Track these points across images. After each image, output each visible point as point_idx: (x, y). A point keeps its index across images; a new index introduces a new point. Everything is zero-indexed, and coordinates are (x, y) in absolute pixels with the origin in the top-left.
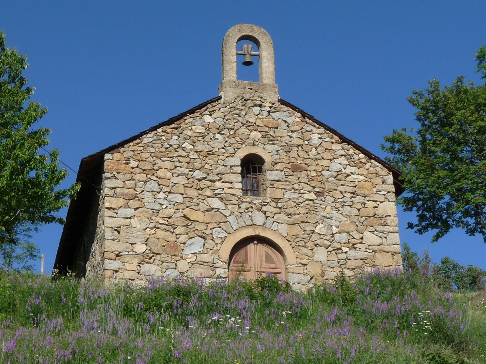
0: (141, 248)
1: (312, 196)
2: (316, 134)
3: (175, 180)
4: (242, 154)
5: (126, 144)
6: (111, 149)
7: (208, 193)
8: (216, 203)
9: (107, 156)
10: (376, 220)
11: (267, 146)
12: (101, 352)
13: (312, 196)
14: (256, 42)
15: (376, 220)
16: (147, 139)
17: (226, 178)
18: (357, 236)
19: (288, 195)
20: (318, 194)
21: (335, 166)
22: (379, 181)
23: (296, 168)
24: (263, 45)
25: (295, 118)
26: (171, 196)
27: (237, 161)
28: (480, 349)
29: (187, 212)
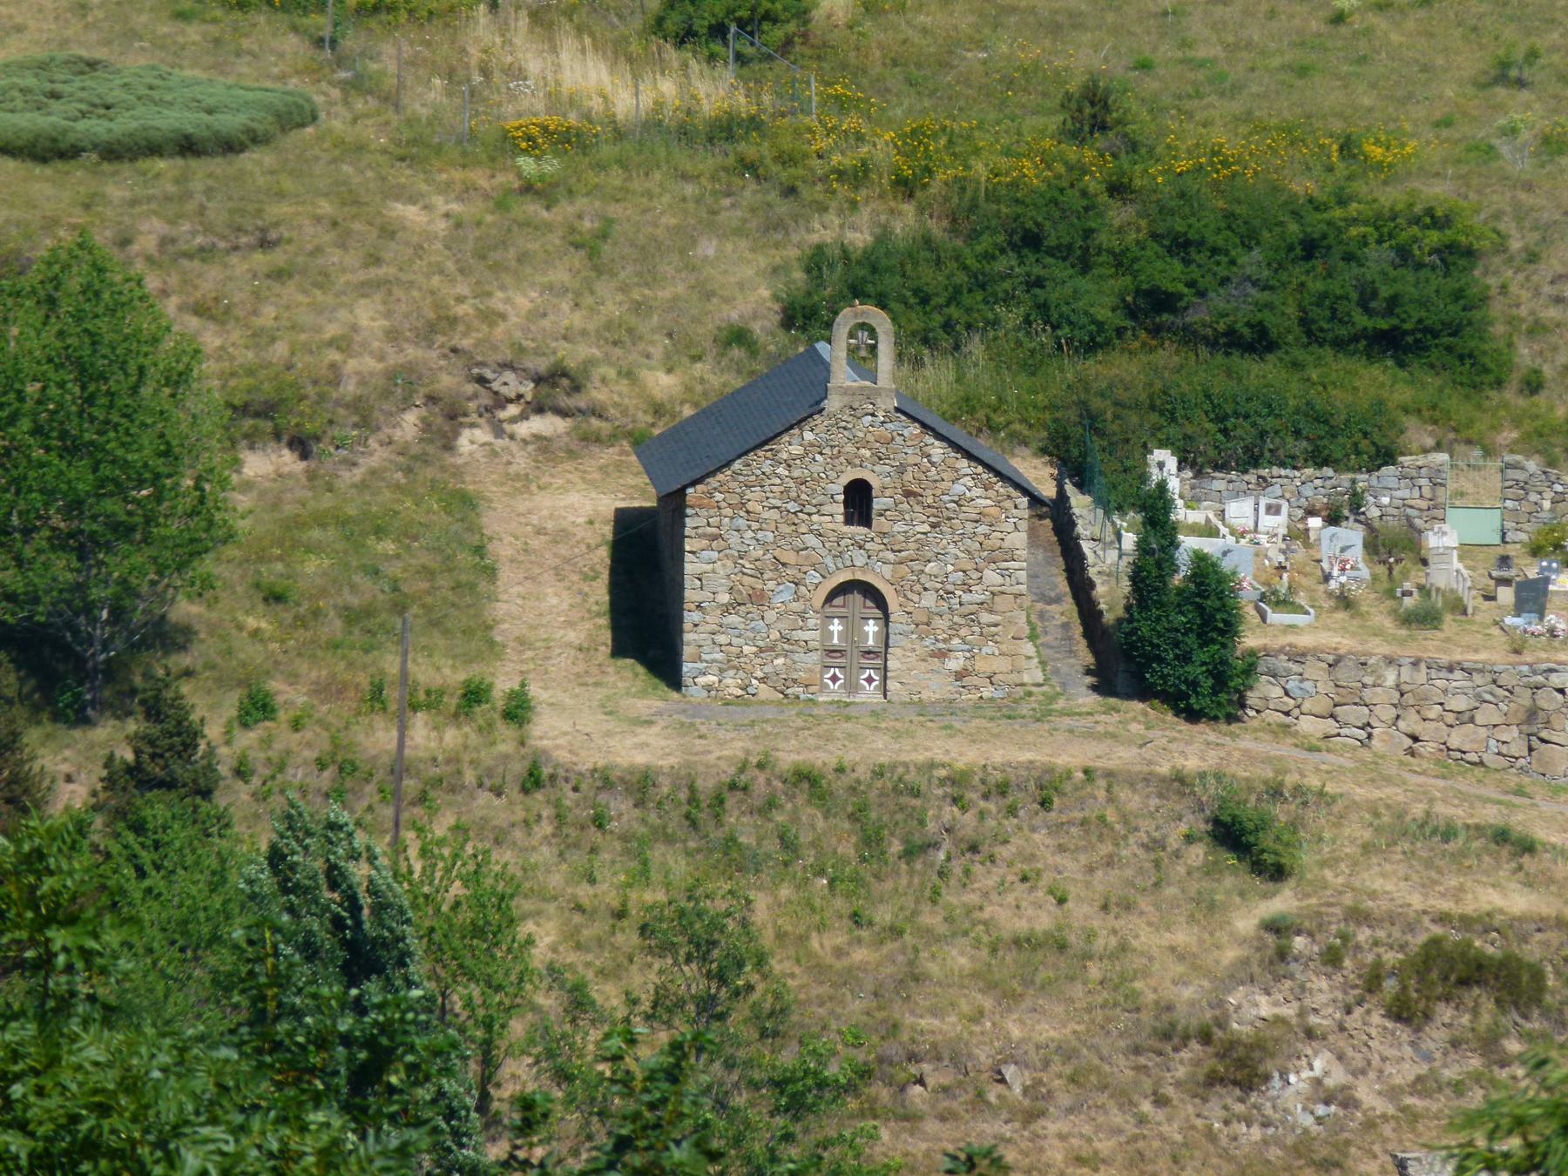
0: (724, 598)
1: (926, 528)
2: (938, 450)
3: (766, 515)
4: (845, 479)
5: (1083, 569)
6: (693, 484)
7: (803, 529)
8: (812, 540)
9: (690, 491)
10: (998, 556)
11: (877, 468)
12: (60, 870)
13: (926, 528)
14: (873, 333)
15: (998, 556)
16: (737, 465)
17: (825, 509)
18: (975, 575)
19: (896, 528)
20: (933, 526)
21: (958, 488)
22: (1008, 504)
23: (908, 494)
24: (882, 337)
25: (915, 429)
26: (760, 535)
27: (838, 488)
28: (1417, 341)
29: (777, 553)
